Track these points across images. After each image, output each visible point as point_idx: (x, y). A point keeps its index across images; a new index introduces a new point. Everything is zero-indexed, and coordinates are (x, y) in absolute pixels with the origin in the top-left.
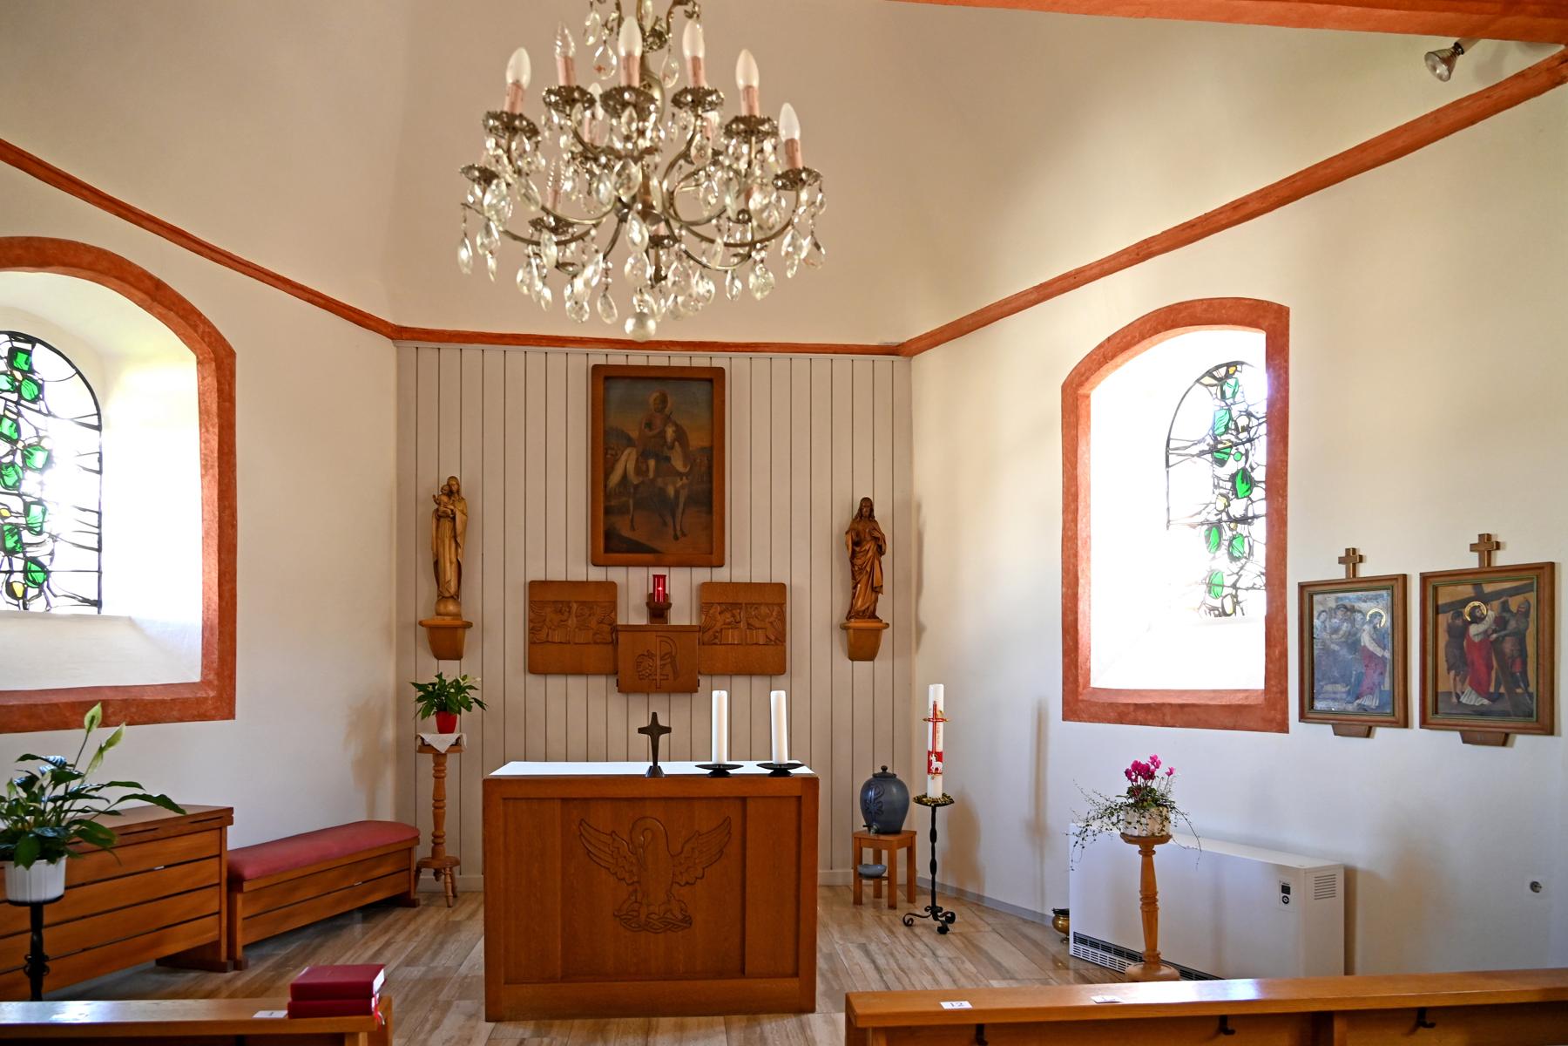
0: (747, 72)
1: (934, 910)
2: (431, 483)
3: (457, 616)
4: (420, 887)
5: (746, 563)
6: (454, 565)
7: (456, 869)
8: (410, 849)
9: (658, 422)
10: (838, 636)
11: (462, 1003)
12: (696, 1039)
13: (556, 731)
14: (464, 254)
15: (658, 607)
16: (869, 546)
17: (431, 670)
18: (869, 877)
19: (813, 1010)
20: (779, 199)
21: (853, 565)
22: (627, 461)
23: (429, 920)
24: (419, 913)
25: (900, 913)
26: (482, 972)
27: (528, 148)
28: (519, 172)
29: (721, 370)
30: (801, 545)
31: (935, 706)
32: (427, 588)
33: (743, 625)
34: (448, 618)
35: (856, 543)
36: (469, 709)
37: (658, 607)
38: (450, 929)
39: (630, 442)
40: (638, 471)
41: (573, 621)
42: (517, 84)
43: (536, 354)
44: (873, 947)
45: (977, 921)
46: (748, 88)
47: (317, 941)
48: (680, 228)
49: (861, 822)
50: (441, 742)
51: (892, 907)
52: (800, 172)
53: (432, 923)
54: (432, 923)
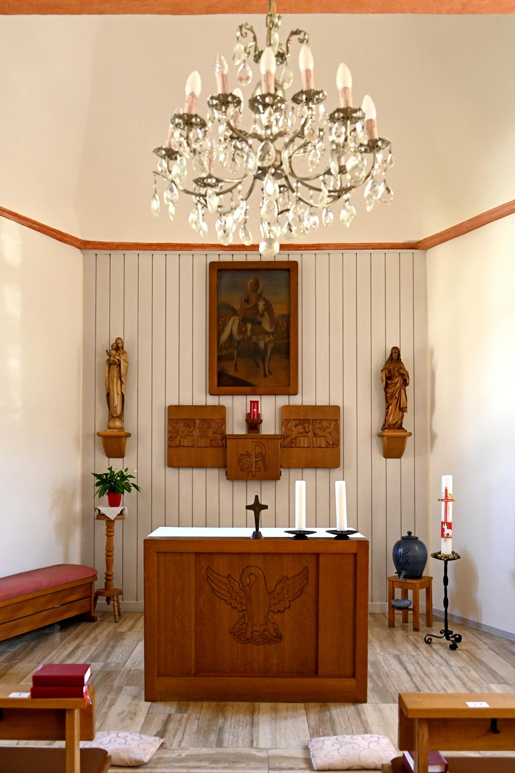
0: (344, 77)
1: (447, 633)
2: (105, 343)
3: (122, 429)
4: (98, 608)
5: (313, 392)
6: (120, 396)
7: (120, 597)
8: (91, 584)
9: (253, 298)
10: (376, 440)
11: (129, 688)
12: (286, 718)
13: (200, 508)
14: (155, 205)
15: (253, 422)
16: (398, 380)
17: (104, 465)
18: (399, 608)
19: (365, 701)
20: (362, 159)
21: (386, 393)
22: (232, 325)
23: (103, 631)
24: (97, 626)
25: (422, 634)
26: (142, 667)
27: (200, 136)
28: (194, 151)
29: (295, 263)
30: (350, 378)
31: (446, 491)
32: (102, 411)
33: (310, 434)
34: (115, 431)
35: (388, 378)
36: (129, 490)
37: (253, 422)
38: (117, 637)
39: (234, 312)
40: (241, 331)
41: (196, 433)
42: (193, 95)
43: (172, 256)
44: (404, 658)
45: (477, 641)
46: (345, 89)
47: (33, 643)
48: (297, 182)
49: (393, 571)
50: (112, 512)
51: (416, 629)
52: (377, 141)
53: (105, 633)
54: (105, 633)
